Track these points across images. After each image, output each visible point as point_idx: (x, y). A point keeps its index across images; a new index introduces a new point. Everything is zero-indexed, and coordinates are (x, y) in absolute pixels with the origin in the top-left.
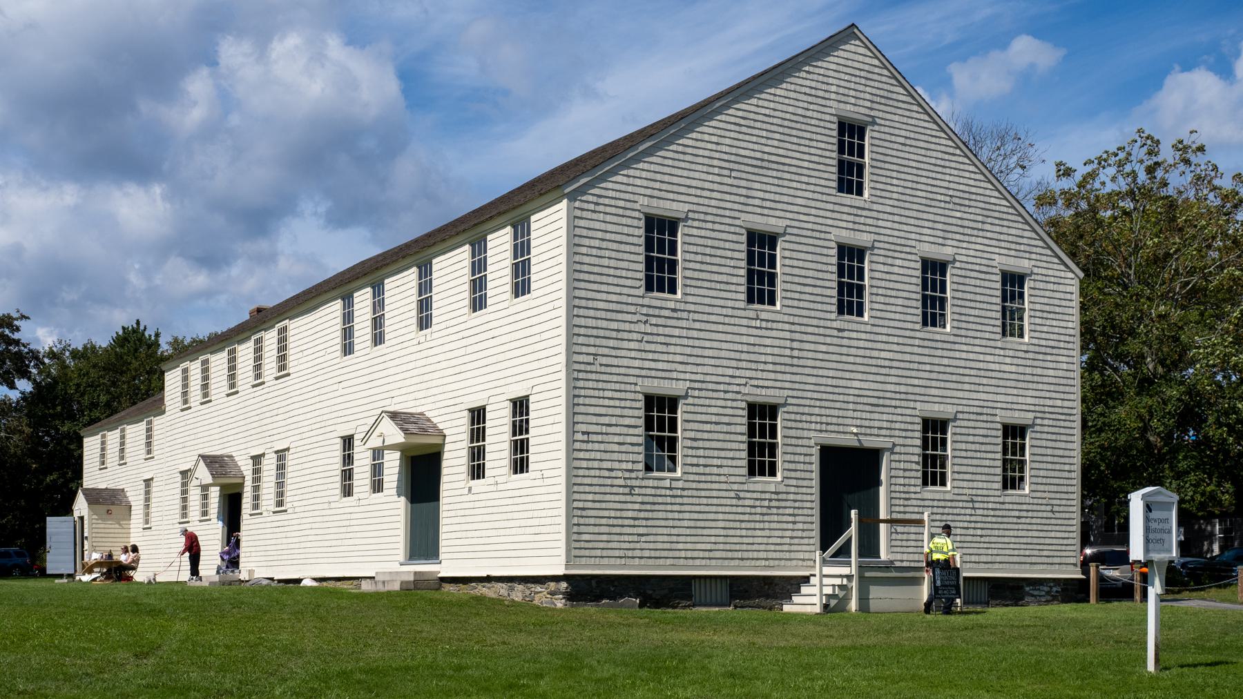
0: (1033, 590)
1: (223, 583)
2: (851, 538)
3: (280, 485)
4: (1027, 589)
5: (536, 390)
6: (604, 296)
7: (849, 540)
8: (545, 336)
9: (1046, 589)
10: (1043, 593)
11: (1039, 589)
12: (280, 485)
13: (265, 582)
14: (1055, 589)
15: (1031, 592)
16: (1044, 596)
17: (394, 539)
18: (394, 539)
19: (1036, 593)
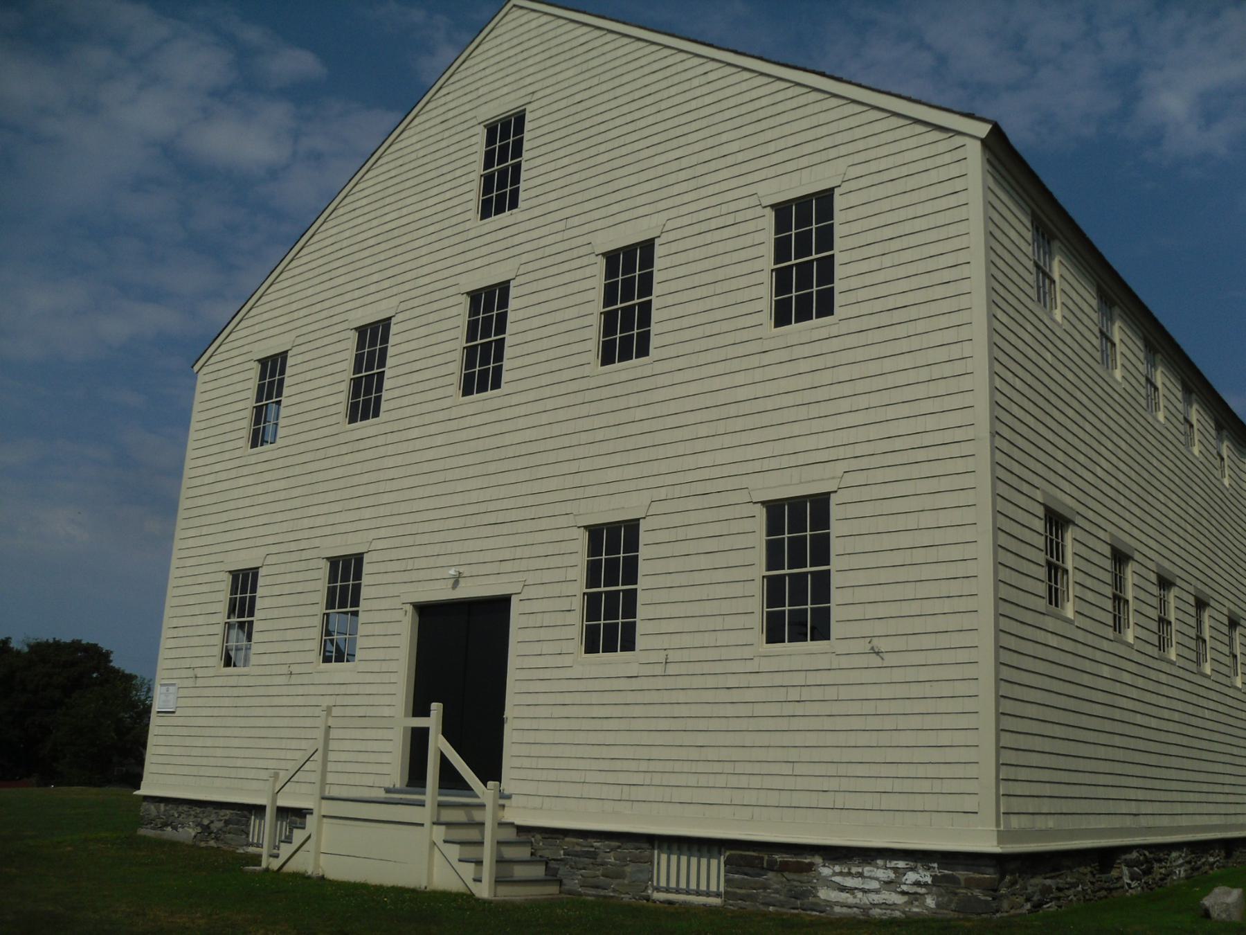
0: (841, 874)
1: (193, 846)
2: (443, 756)
3: (1127, 334)
4: (826, 871)
5: (270, 560)
6: (945, 518)
7: (444, 760)
8: (420, 539)
9: (882, 874)
10: (875, 885)
11: (861, 875)
12: (1127, 334)
13: (702, 906)
14: (911, 877)
15: (837, 879)
16: (877, 891)
17: (740, 542)
18: (740, 542)
19: (850, 882)
